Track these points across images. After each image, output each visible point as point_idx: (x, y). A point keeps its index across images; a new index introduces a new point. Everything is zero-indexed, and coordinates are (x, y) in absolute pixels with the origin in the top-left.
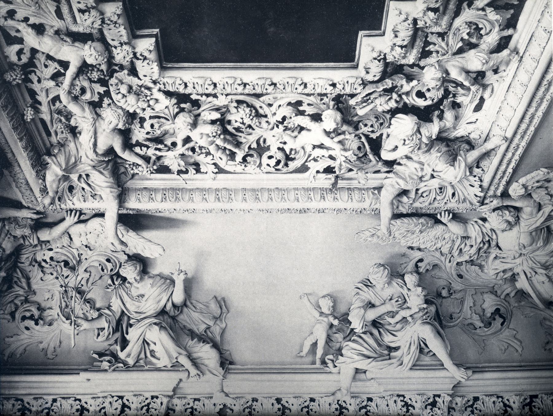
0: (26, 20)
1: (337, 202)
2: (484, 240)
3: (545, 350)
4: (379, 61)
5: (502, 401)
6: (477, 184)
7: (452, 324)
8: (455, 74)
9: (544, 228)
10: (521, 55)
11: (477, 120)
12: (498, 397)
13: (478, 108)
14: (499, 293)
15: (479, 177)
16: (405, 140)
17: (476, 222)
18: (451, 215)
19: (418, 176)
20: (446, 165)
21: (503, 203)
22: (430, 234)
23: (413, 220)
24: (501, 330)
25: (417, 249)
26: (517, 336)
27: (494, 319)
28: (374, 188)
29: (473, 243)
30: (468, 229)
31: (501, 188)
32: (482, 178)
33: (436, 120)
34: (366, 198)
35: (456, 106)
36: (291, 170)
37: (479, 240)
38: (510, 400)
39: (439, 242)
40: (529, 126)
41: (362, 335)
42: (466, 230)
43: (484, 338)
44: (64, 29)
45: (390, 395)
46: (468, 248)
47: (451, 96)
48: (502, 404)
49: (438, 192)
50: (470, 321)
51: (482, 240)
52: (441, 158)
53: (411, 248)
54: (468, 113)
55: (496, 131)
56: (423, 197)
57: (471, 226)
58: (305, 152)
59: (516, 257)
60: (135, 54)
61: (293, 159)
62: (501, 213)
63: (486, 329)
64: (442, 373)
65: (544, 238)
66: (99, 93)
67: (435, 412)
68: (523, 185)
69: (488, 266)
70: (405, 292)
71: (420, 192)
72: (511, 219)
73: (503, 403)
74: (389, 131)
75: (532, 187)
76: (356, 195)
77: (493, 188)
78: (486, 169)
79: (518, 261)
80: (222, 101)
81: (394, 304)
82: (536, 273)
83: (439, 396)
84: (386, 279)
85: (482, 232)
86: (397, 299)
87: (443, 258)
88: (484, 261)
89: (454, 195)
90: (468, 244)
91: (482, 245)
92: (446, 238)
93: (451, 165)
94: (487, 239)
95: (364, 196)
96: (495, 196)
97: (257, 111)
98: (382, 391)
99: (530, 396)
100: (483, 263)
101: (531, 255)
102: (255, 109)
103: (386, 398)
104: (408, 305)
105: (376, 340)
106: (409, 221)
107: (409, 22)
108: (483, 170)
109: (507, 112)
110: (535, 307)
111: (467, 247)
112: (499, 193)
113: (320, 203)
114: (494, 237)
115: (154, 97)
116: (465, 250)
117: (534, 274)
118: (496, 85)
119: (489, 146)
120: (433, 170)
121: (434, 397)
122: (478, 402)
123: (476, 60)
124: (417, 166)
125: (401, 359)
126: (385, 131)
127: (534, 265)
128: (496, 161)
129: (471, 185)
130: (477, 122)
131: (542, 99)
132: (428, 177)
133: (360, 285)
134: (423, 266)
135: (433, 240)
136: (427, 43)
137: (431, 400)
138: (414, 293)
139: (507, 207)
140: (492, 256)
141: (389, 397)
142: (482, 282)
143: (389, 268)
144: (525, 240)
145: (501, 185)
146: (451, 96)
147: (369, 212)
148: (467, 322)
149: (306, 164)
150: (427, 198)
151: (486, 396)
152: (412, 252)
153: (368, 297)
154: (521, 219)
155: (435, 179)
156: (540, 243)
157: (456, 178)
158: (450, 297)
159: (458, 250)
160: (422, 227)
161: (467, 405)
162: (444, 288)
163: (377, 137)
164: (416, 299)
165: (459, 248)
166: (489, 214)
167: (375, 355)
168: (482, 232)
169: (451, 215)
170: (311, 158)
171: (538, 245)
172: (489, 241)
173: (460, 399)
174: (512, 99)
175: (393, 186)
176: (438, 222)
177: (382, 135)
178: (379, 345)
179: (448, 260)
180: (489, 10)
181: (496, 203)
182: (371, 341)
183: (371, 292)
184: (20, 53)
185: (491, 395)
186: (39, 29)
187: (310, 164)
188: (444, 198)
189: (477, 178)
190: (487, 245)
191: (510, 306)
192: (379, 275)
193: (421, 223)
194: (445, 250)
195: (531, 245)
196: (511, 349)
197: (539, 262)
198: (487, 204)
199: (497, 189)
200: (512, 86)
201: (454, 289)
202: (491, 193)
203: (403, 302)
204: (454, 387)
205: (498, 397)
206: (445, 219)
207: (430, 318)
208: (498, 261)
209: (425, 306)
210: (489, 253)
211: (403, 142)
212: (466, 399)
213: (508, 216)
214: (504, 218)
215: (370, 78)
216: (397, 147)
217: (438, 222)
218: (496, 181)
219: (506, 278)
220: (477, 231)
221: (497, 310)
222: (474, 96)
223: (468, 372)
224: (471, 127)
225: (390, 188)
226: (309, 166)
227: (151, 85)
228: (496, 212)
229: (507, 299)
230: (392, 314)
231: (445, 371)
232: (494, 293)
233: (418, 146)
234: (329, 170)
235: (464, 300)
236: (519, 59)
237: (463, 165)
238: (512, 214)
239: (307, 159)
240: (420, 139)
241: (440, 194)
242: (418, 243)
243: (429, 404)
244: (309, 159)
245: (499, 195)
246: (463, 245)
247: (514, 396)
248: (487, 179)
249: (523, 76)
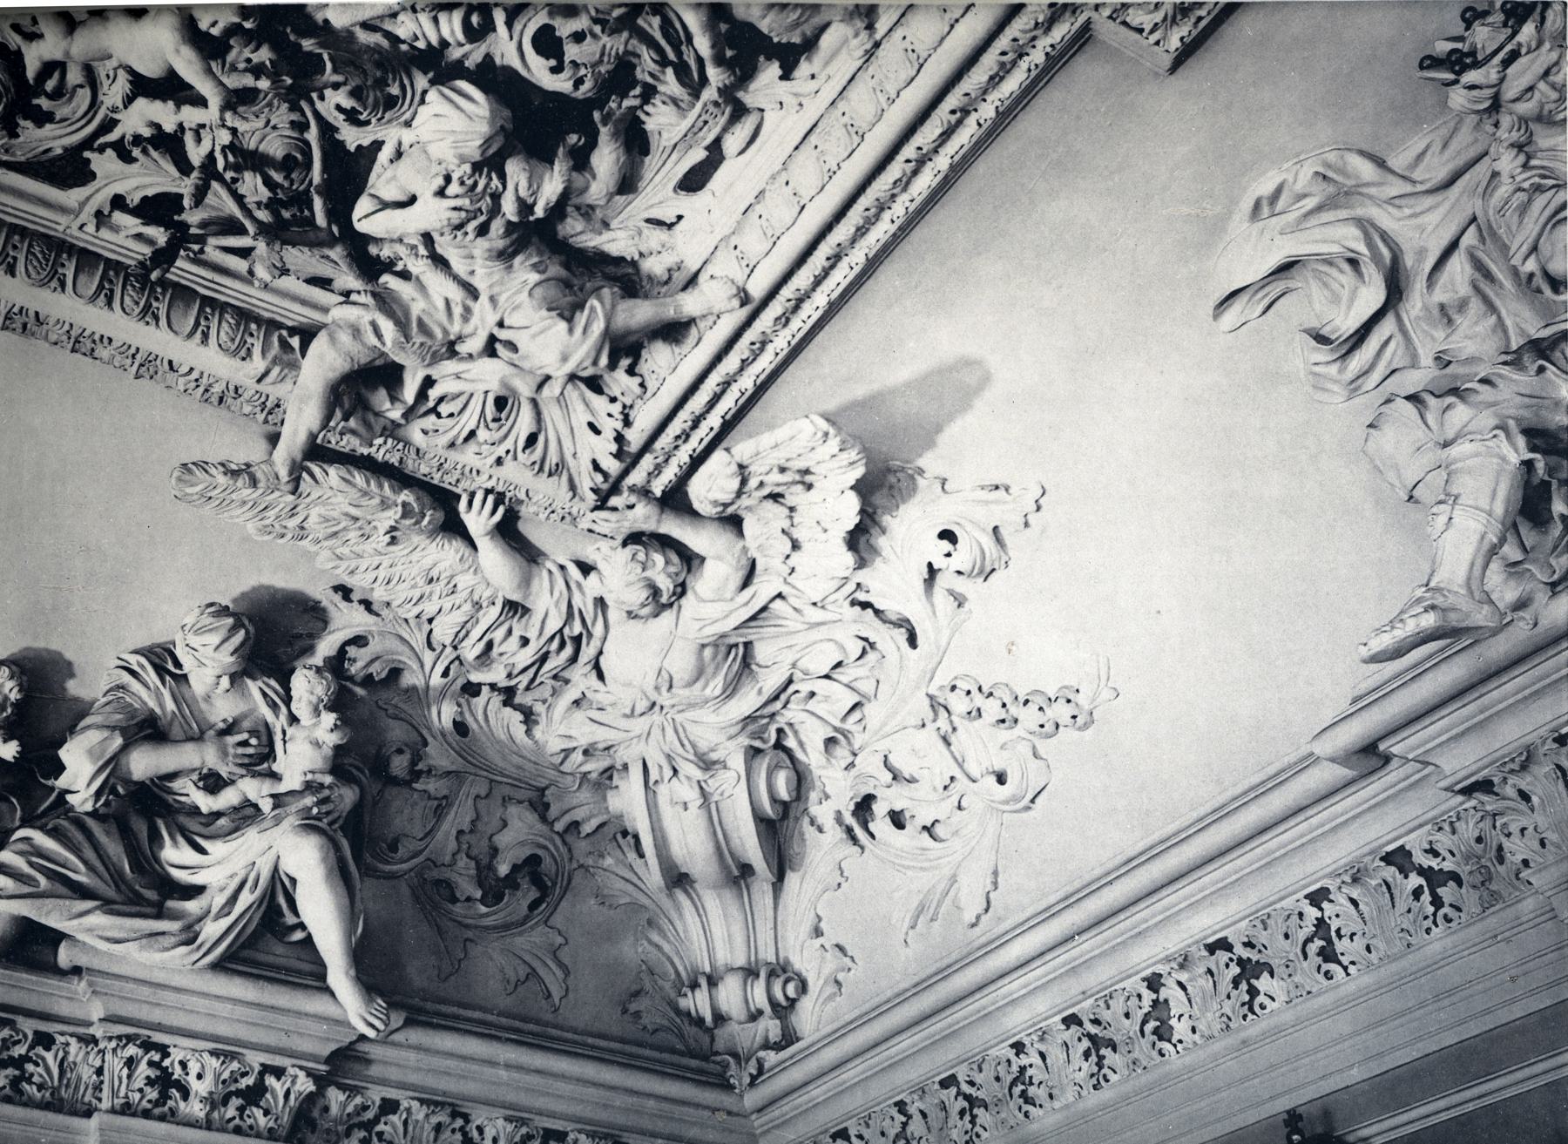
1: (152, 328)
2: (566, 631)
3: (625, 1011)
5: (462, 1129)
6: (610, 426)
7: (388, 868)
9: (736, 645)
10: (878, 36)
11: (680, 218)
12: (455, 1114)
13: (694, 181)
14: (553, 812)
15: (624, 407)
16: (448, 179)
17: (562, 567)
18: (501, 510)
19: (446, 332)
20: (544, 313)
21: (659, 521)
22: (415, 556)
23: (381, 487)
24: (526, 919)
25: (361, 602)
26: (562, 955)
27: (516, 887)
28: (293, 331)
29: (532, 634)
30: (535, 583)
31: (670, 474)
32: (632, 414)
34: (257, 351)
35: (636, 141)
36: (20, 157)
37: (553, 625)
38: (487, 1130)
39: (435, 597)
40: (818, 282)
41: (90, 822)
42: (526, 582)
43: (470, 934)
45: (119, 1038)
46: (514, 641)
47: (638, 91)
48: (459, 1136)
49: (489, 417)
50: (446, 874)
51: (561, 631)
52: (539, 291)
53: (345, 592)
54: (661, 175)
55: (727, 266)
56: (439, 416)
57: (545, 574)
58: (94, 104)
59: (638, 710)
61: (43, 118)
62: (641, 556)
63: (484, 909)
64: (315, 1004)
65: (731, 676)
67: (250, 1121)
68: (741, 467)
69: (550, 720)
70: (279, 723)
71: (433, 394)
72: (666, 585)
73: (465, 1134)
74: (407, 136)
75: (762, 484)
76: (222, 330)
77: (647, 462)
78: (652, 385)
79: (639, 725)
81: (231, 751)
82: (675, 771)
83: (279, 1072)
84: (232, 659)
85: (570, 606)
86: (245, 736)
87: (428, 657)
88: (544, 701)
89: (532, 440)
90: (517, 633)
91: (555, 645)
92: (460, 587)
93: (561, 316)
94: (577, 628)
95: (250, 340)
96: (645, 492)
98: (95, 1017)
99: (545, 1130)
100: (539, 708)
101: (679, 718)
103: (102, 1045)
104: (275, 767)
105: (133, 851)
106: (368, 482)
108: (642, 385)
109: (778, 209)
110: (635, 880)
111: (511, 639)
112: (658, 488)
113: (90, 308)
114: (598, 630)
116: (502, 649)
117: (668, 773)
118: (769, 117)
119: (690, 304)
120: (501, 324)
121: (261, 1074)
122: (394, 1118)
124: (456, 294)
125: (197, 928)
126: (391, 134)
127: (680, 750)
128: (694, 357)
129: (591, 426)
130: (678, 228)
131: (882, 207)
132: (475, 344)
133: (134, 661)
134: (359, 662)
135: (421, 582)
137: (249, 1081)
138: (306, 733)
139: (666, 543)
140: (572, 694)
141: (113, 1044)
142: (519, 767)
143: (251, 629)
144: (681, 663)
145: (674, 462)
146: (638, 91)
147: (247, 409)
148: (435, 874)
149: (87, 154)
150: (450, 422)
151: (422, 1101)
152: (343, 605)
153: (152, 704)
154: (690, 594)
155: (495, 360)
156: (716, 685)
157: (565, 359)
158: (411, 781)
159: (482, 645)
160: (404, 516)
161: (356, 1120)
162: (400, 751)
163: (359, 147)
164: (306, 748)
165: (486, 639)
166: (609, 552)
167: (110, 892)
168: (570, 606)
169: (501, 510)
170: (113, 136)
171: (708, 692)
172: (577, 640)
173: (342, 1097)
174: (806, 173)
175: (356, 332)
176: (453, 527)
177: (378, 145)
178: (136, 866)
179: (440, 668)
181: (643, 516)
182: (114, 848)
183: (166, 694)
185: (436, 1104)
187: (104, 163)
188: (506, 436)
189: (616, 409)
190: (568, 650)
191: (571, 859)
192: (215, 639)
193: (405, 505)
194: (444, 631)
195: (691, 684)
196: (532, 985)
197: (694, 746)
198: (615, 509)
199: (658, 469)
200: (817, 130)
201: (432, 762)
202: (637, 477)
203: (261, 760)
204: (334, 1054)
205: (455, 1114)
206: (478, 521)
207: (330, 818)
208: (579, 715)
209: (328, 780)
210: (567, 682)
211: (440, 181)
212: (358, 1100)
213: (661, 569)
214: (648, 573)
216: (413, 200)
217: (453, 527)
218: (665, 441)
219: (585, 774)
220: (556, 594)
221: (534, 860)
222: (700, 124)
223: (393, 1016)
224: (656, 237)
225: (344, 337)
226: (93, 167)
228: (631, 548)
229: (569, 838)
230: (213, 783)
231: (326, 998)
232: (540, 808)
233: (482, 219)
234: (159, 209)
235: (450, 805)
236: (868, 46)
237: (598, 327)
238: (672, 569)
240: (496, 197)
241: (491, 425)
242: (371, 576)
243: (238, 1093)
244: (102, 140)
245: (658, 493)
246: (498, 635)
247: (500, 1122)
248: (645, 419)
249: (861, 102)
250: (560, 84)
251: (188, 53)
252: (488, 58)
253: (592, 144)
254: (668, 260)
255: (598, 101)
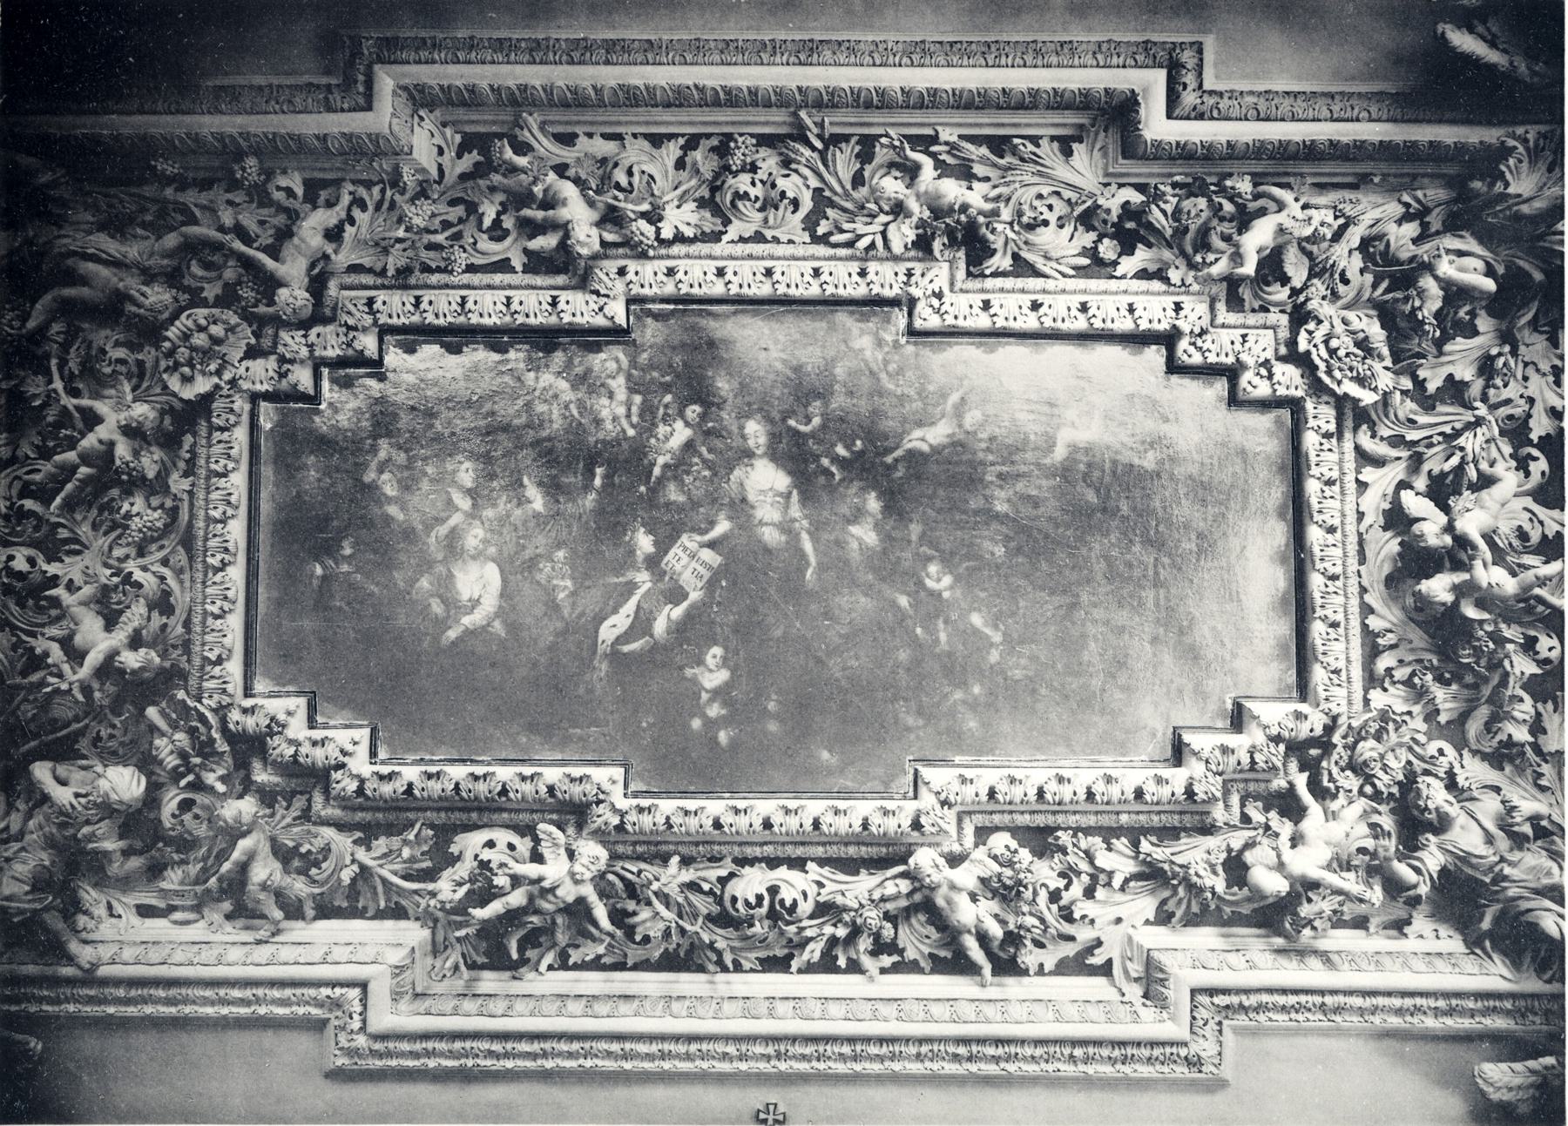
0: (352, 221)
4: (268, 726)
8: (244, 844)
23: (1269, 485)
33: (122, 844)
44: (330, 268)
60: (292, 361)
66: (202, 289)
80: (178, 484)
97: (153, 540)
102: (160, 538)
107: (341, 758)
115: (199, 378)
118: (202, 924)
123: (268, 871)
130: (113, 920)
136: (290, 797)
177: (85, 757)
180: (355, 868)
184: (290, 192)
186: (334, 235)
215: (235, 715)
224: (101, 911)
227: (227, 376)
239: (22, 630)
249: (235, 954)
250: (167, 822)
251: (101, 657)
252: (748, 454)
253: (140, 853)
254: (91, 924)
255: (168, 841)
